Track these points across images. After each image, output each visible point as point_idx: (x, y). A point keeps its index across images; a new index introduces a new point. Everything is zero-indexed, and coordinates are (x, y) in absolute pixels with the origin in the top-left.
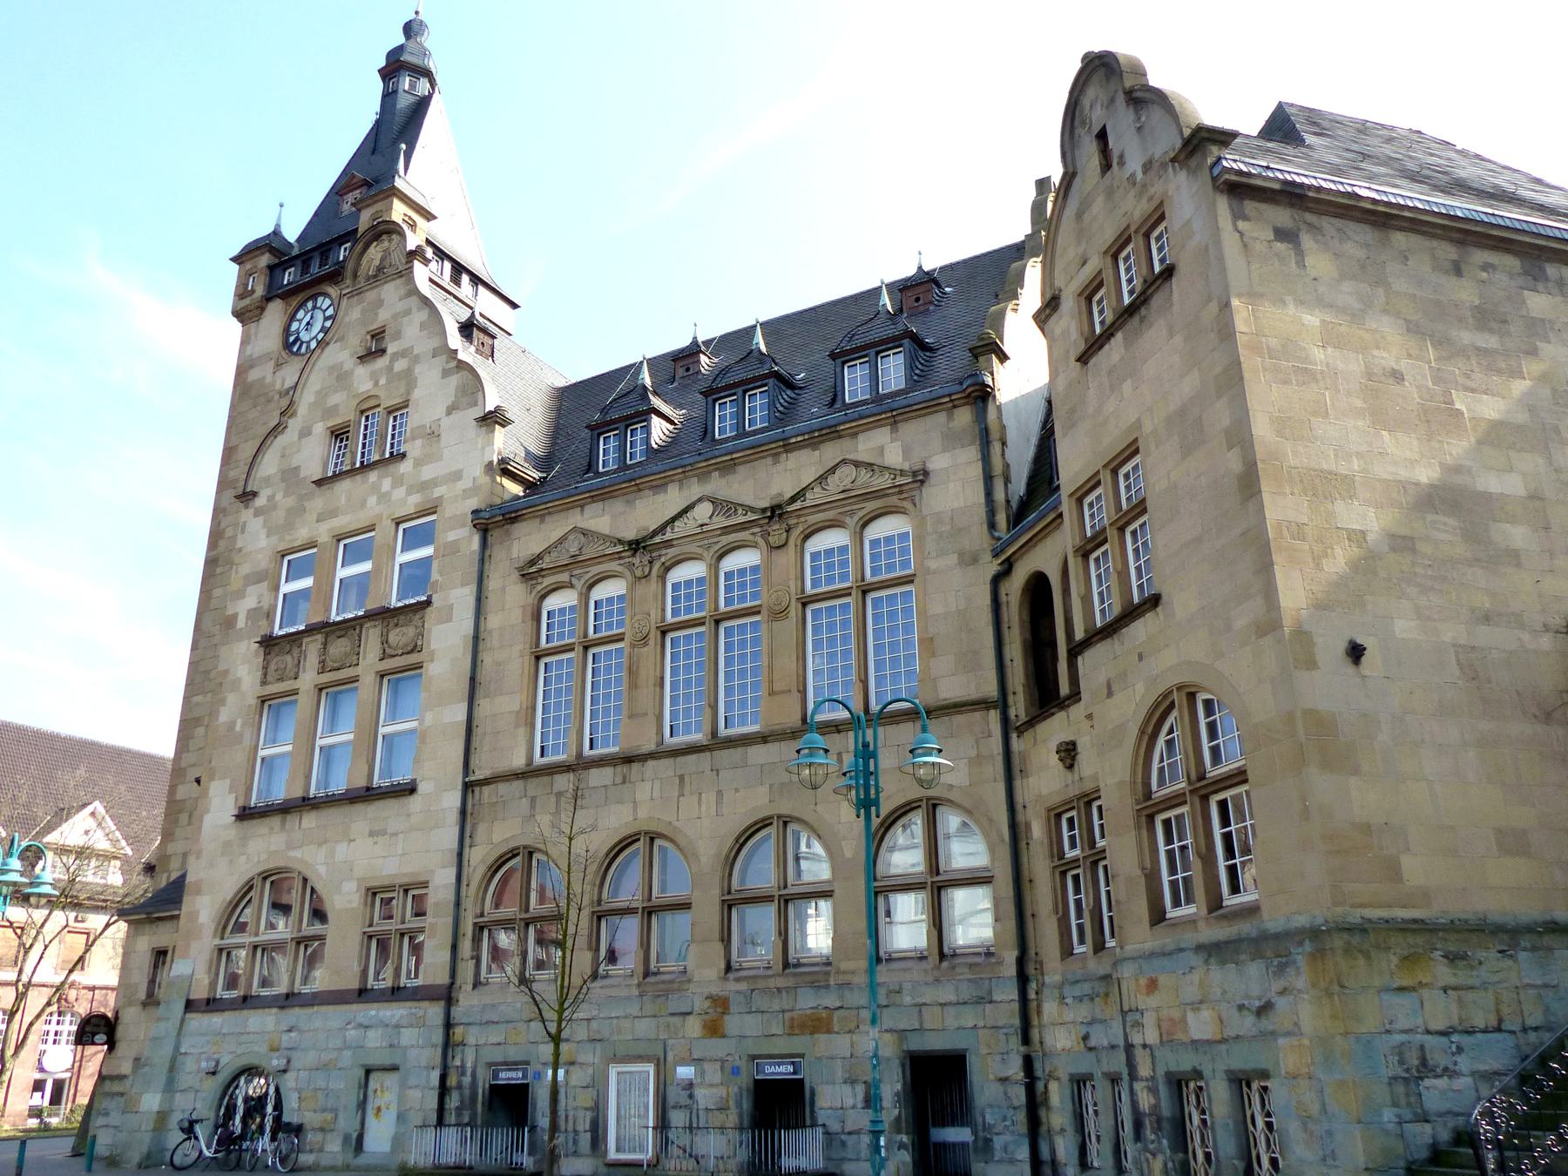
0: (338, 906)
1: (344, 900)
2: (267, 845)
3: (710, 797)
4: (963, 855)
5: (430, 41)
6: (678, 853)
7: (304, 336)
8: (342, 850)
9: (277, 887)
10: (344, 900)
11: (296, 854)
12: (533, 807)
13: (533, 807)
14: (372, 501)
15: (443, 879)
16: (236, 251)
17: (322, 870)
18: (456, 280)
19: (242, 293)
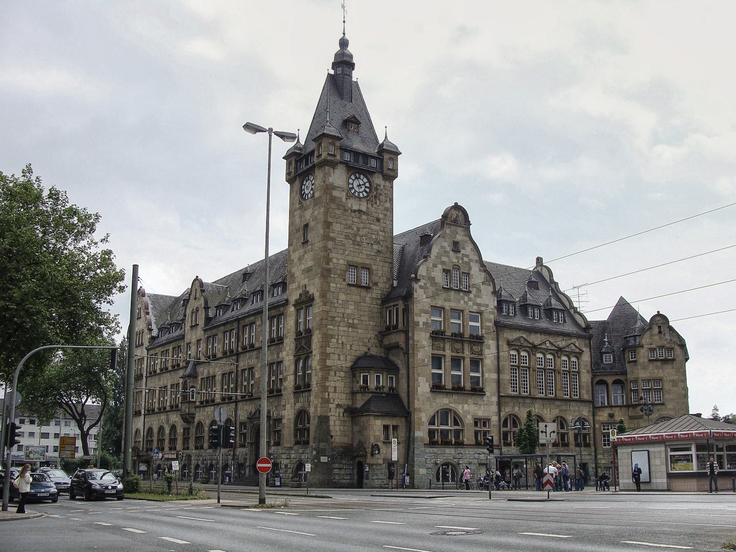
0: (467, 422)
1: (469, 420)
2: (444, 401)
3: (549, 410)
4: (51, 487)
5: (351, 49)
6: (143, 419)
7: (307, 192)
8: (466, 406)
9: (445, 414)
10: (469, 420)
11: (453, 405)
12: (514, 404)
13: (514, 404)
14: (462, 302)
15: (494, 419)
16: (284, 154)
17: (461, 411)
18: (356, 161)
19: (288, 174)
